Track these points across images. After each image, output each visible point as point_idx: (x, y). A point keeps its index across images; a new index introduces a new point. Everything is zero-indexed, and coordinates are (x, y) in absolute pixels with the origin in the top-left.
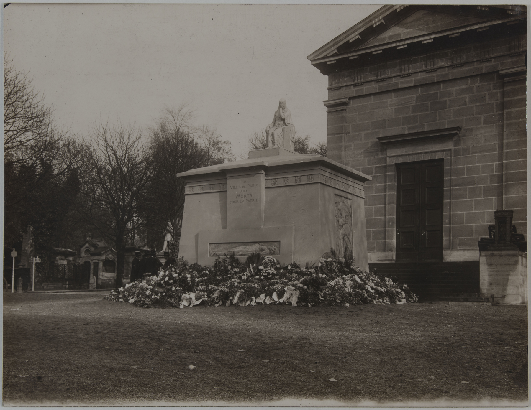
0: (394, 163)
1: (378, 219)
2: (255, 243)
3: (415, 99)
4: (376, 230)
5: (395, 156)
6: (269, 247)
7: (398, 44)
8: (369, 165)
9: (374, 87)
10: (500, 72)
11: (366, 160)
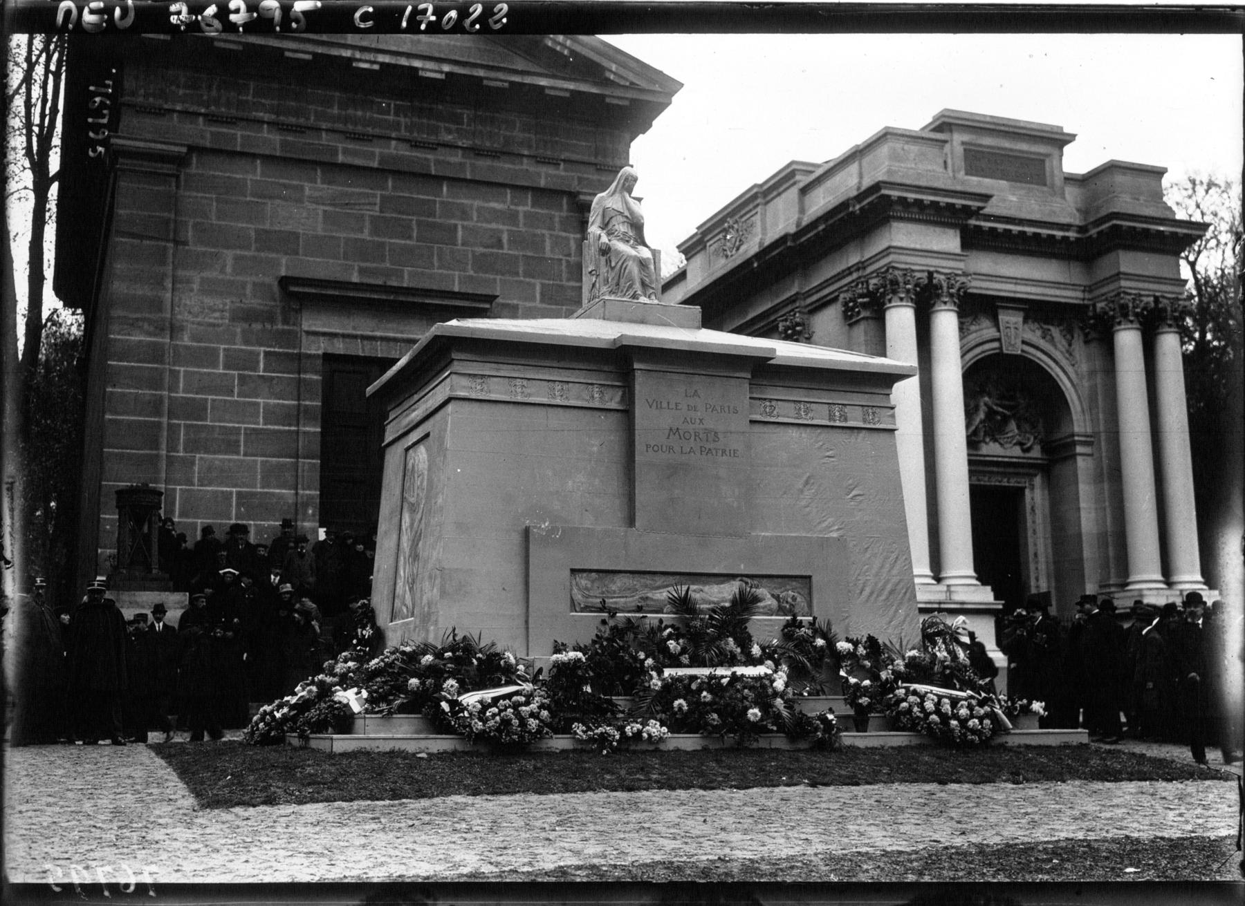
0: (320, 352)
1: (273, 494)
2: (733, 577)
3: (378, 201)
4: (266, 524)
5: (324, 334)
6: (776, 592)
7: (358, 55)
8: (246, 342)
9: (271, 140)
10: (582, 197)
11: (239, 330)
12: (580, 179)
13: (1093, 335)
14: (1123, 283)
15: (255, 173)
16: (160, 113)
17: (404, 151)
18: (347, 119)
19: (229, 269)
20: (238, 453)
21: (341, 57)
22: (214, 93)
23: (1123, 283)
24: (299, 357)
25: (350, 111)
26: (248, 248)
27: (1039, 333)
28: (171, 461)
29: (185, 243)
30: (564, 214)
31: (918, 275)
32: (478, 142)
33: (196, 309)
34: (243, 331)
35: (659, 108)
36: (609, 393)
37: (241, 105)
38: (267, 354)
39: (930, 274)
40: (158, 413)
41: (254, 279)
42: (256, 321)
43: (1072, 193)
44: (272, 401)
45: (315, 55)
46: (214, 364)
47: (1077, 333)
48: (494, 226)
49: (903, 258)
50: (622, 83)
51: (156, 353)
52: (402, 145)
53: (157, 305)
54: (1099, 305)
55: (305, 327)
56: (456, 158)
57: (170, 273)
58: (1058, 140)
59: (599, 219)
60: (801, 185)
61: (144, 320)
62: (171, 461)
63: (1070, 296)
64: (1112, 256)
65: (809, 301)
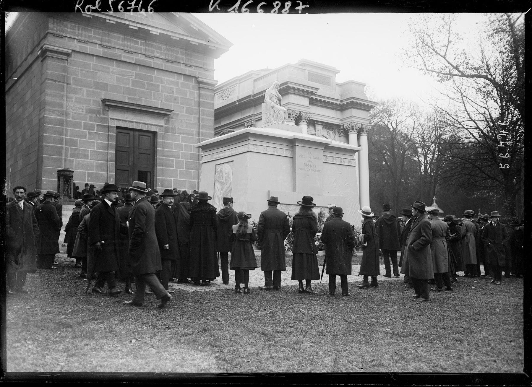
0: (115, 126)
5: (117, 119)
7: (131, 24)
12: (199, 73)
13: (342, 134)
14: (353, 119)
15: (93, 61)
16: (61, 37)
17: (143, 58)
18: (124, 46)
19: (85, 95)
20: (88, 159)
21: (125, 24)
22: (80, 32)
23: (353, 119)
24: (108, 126)
25: (126, 43)
26: (91, 88)
27: (326, 133)
28: (66, 160)
29: (70, 84)
30: (193, 84)
31: (297, 112)
32: (167, 57)
33: (74, 108)
34: (90, 117)
35: (224, 51)
36: (288, 152)
37: (89, 37)
38: (97, 125)
39: (300, 112)
40: (61, 144)
41: (93, 98)
42: (94, 113)
43: (338, 88)
44: (99, 142)
45: (117, 22)
46: (80, 128)
47: (337, 133)
48: (171, 86)
49: (293, 107)
50: (214, 42)
51: (61, 123)
52: (142, 56)
53: (61, 105)
54: (345, 125)
55: (110, 117)
56: (160, 62)
57: (65, 94)
58: (336, 72)
59: (269, 97)
60: (254, 79)
61: (57, 110)
62: (66, 160)
63: (337, 122)
64: (350, 110)
65: (256, 117)
